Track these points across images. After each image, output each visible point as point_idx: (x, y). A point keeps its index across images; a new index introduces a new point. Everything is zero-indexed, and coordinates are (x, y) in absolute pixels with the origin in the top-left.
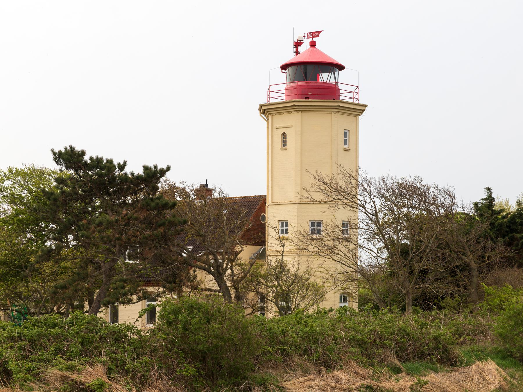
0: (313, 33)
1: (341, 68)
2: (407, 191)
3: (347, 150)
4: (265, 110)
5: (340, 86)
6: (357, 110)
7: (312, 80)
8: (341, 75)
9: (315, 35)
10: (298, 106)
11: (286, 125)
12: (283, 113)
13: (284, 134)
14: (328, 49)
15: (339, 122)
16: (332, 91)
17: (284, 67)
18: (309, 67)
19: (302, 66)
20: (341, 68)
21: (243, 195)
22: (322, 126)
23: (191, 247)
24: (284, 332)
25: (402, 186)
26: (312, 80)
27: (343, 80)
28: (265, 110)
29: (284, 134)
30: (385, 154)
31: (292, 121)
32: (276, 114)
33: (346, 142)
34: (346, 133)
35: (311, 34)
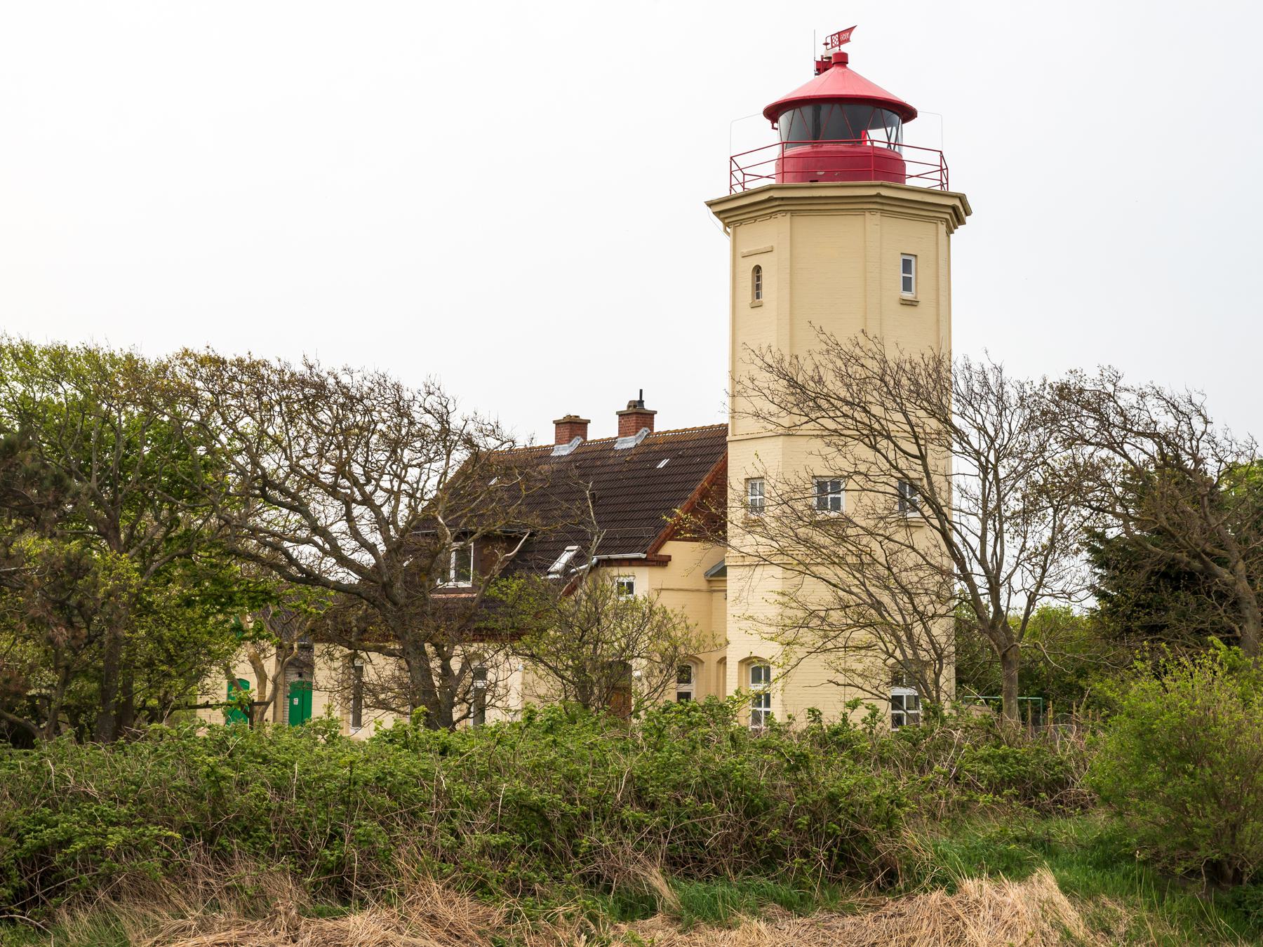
0: (839, 33)
1: (907, 113)
2: (1067, 405)
3: (912, 303)
4: (734, 211)
5: (906, 154)
6: (955, 212)
7: (840, 140)
8: (909, 131)
9: (842, 38)
10: (782, 199)
11: (761, 247)
12: (755, 219)
13: (758, 269)
14: (873, 70)
15: (883, 237)
16: (888, 166)
17: (773, 113)
18: (825, 109)
19: (808, 111)
20: (907, 113)
21: (708, 424)
22: (846, 249)
23: (575, 547)
24: (162, 369)
25: (1063, 392)
26: (840, 140)
27: (916, 146)
28: (734, 211)
29: (758, 269)
30: (1016, 314)
31: (772, 232)
32: (741, 222)
33: (907, 285)
34: (907, 266)
35: (836, 38)
